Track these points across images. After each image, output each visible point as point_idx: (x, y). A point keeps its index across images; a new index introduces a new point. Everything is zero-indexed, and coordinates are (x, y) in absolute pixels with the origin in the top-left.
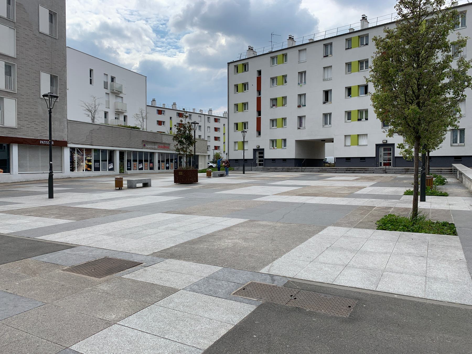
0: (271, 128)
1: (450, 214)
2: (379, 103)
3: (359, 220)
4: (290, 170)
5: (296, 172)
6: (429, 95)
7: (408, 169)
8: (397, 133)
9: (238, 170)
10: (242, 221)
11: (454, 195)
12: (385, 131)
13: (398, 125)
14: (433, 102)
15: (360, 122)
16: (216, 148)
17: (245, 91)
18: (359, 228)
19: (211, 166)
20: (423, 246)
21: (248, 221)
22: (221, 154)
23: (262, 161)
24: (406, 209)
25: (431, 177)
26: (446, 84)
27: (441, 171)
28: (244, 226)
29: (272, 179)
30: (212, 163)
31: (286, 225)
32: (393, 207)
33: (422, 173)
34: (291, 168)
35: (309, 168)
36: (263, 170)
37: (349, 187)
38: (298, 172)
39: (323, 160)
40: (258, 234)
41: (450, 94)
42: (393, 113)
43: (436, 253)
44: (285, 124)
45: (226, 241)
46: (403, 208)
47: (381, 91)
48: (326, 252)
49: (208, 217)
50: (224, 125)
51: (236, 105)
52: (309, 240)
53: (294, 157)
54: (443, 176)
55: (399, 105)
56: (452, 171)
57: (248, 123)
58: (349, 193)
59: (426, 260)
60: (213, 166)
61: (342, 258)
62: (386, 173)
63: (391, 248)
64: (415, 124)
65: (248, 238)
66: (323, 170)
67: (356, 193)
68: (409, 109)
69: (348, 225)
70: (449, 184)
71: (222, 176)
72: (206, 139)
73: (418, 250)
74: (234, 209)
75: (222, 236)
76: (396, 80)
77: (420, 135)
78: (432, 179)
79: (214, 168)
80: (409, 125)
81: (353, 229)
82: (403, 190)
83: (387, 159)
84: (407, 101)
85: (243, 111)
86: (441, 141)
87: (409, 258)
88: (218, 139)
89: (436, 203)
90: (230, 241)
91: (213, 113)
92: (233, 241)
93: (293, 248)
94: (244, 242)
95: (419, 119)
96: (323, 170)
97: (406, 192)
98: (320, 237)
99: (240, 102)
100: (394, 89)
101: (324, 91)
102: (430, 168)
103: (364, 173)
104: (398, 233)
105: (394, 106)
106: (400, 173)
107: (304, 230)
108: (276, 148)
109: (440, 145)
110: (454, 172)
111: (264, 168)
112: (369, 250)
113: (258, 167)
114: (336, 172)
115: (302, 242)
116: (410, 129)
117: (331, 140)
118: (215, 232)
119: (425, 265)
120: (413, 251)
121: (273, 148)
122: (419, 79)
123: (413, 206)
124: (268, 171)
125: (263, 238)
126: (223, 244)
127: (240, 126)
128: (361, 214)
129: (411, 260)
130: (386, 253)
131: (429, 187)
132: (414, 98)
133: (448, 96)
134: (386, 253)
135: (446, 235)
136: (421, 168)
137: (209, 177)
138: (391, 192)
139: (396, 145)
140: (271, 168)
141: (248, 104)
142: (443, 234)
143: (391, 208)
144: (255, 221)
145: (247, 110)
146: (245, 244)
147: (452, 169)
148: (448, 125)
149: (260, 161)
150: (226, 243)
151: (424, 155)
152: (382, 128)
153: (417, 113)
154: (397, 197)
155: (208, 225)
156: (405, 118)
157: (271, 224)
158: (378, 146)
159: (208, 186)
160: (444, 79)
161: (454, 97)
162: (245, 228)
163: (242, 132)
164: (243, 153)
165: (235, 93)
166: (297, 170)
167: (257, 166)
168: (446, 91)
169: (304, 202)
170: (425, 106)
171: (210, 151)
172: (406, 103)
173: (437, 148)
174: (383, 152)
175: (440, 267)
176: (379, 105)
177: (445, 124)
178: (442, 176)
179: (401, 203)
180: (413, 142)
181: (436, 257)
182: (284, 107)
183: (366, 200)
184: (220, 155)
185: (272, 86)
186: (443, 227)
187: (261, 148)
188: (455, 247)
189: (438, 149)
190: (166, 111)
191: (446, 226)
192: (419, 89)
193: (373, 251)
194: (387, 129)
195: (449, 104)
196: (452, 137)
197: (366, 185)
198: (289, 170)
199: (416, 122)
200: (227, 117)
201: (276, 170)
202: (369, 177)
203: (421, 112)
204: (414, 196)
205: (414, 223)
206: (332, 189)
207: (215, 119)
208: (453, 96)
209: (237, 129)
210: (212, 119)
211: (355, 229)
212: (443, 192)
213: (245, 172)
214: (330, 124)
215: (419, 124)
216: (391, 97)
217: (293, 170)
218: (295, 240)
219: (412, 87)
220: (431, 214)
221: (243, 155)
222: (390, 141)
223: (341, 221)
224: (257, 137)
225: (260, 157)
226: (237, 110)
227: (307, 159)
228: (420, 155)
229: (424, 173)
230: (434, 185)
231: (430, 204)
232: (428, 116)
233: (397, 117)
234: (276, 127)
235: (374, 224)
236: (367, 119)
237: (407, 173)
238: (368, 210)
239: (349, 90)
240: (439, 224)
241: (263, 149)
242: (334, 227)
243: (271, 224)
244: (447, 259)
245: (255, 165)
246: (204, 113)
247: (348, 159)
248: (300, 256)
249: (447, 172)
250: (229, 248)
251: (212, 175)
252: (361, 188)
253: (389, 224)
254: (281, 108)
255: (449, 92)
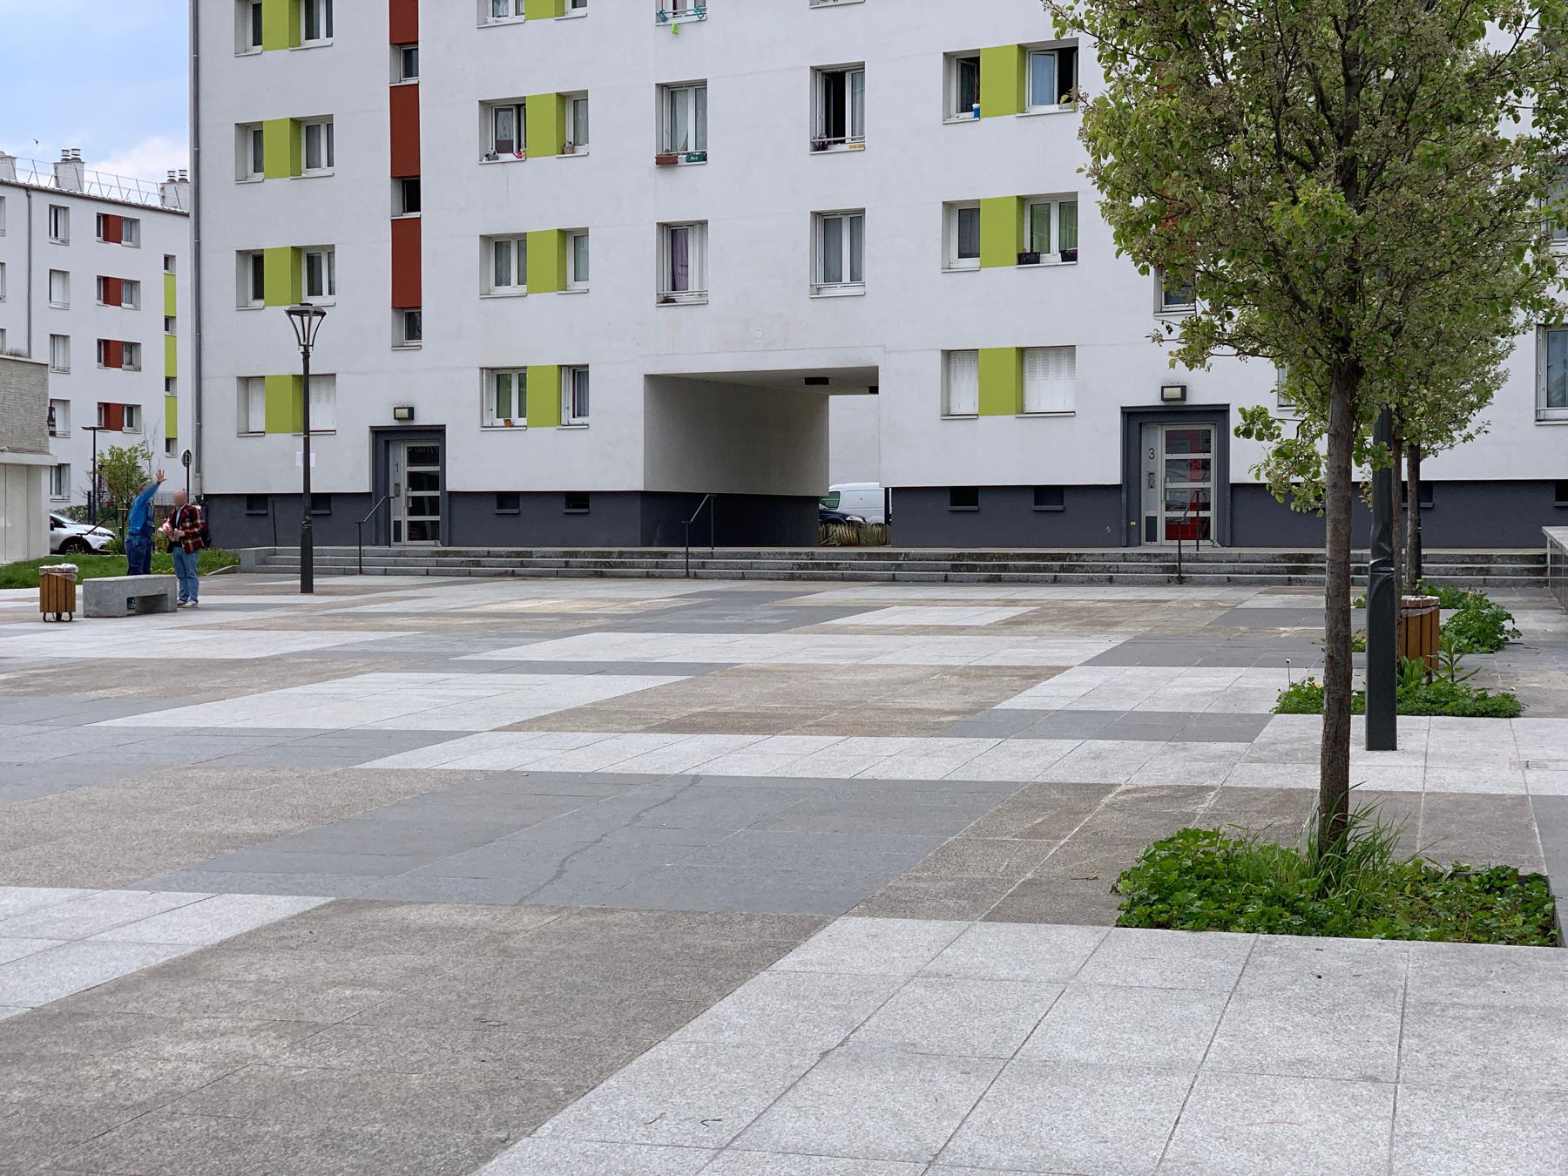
0: (486, 295)
1: (1524, 821)
2: (1124, 161)
3: (1020, 870)
4: (617, 565)
5: (648, 576)
6: (1404, 122)
7: (1306, 558)
8: (1230, 342)
9: (264, 566)
10: (282, 907)
11: (1551, 709)
12: (1166, 335)
13: (1237, 294)
14: (1430, 163)
15: (1029, 271)
16: (113, 416)
17: (311, 43)
18: (1019, 919)
19: (76, 544)
20: (1374, 1012)
21: (322, 907)
22: (148, 457)
23: (433, 506)
24: (1288, 798)
25: (1426, 605)
26: (1500, 60)
27: (1482, 569)
28: (293, 943)
29: (492, 626)
30: (81, 521)
31: (576, 922)
32: (1213, 788)
33: (1373, 579)
34: (621, 554)
35: (734, 556)
36: (440, 570)
37: (965, 673)
38: (661, 577)
39: (816, 500)
40: (389, 993)
41: (1517, 119)
42: (1206, 224)
43: (1448, 1052)
44: (581, 272)
45: (169, 1049)
46: (1268, 793)
47: (1138, 85)
48: (816, 1078)
49: (44, 891)
50: (168, 260)
51: (253, 134)
52: (714, 1009)
53: (633, 480)
54: (1496, 599)
55: (1243, 174)
56: (1542, 571)
57: (331, 255)
58: (968, 707)
59: (1391, 1096)
60: (90, 538)
61: (908, 1114)
62: (1181, 581)
63: (1198, 1036)
64: (1329, 293)
65: (319, 1019)
66: (818, 566)
67: (1005, 705)
68: (1295, 201)
69: (951, 903)
70: (1527, 647)
71: (149, 605)
72: (41, 354)
73: (1346, 1039)
74: (231, 829)
75: (140, 1015)
76: (1220, 22)
77: (1359, 359)
78: (1434, 616)
79: (95, 552)
80: (1297, 299)
81: (980, 927)
82: (1274, 681)
83: (1187, 499)
84: (1286, 154)
85: (296, 173)
86: (1485, 396)
87: (1299, 1091)
88: (126, 357)
89: (1451, 758)
90: (190, 1048)
91: (88, 176)
92: (215, 1044)
93: (612, 1070)
94: (292, 1048)
95: (1351, 261)
96: (818, 566)
97: (1288, 695)
98: (783, 986)
99: (275, 111)
100: (1213, 79)
101: (816, 70)
102: (1424, 552)
103: (1055, 581)
104: (1237, 941)
105: (1213, 182)
106: (1262, 578)
107: (687, 946)
108: (523, 421)
109: (1478, 418)
110: (1555, 572)
111: (446, 554)
112: (1069, 1052)
113: (407, 545)
114: (893, 580)
115: (671, 1028)
116: (1302, 321)
117: (865, 381)
118: (89, 994)
119: (1382, 1127)
120: (1318, 1047)
121: (501, 422)
122: (1351, 21)
123: (1323, 779)
124: (472, 570)
125: (420, 1018)
126: (143, 1073)
127: (277, 274)
128: (1034, 833)
129: (1306, 1106)
130: (1169, 1068)
131: (1413, 666)
132: (1328, 136)
133: (1507, 130)
134: (1169, 1068)
135: (1501, 947)
136: (1369, 551)
137: (59, 619)
138: (1206, 694)
139: (1236, 420)
140: (489, 554)
141: (330, 127)
142: (1488, 941)
143: (1202, 790)
144: (371, 904)
145: (329, 171)
146: (293, 1062)
147: (1545, 556)
148: (1509, 304)
149: (417, 506)
150: (168, 1060)
151: (1385, 476)
152: (1159, 311)
153: (1336, 229)
154: (1242, 727)
155: (39, 945)
156: (1275, 255)
157: (482, 917)
158: (1135, 419)
159: (47, 680)
160: (1484, 32)
161: (1538, 142)
162: (302, 959)
163: (290, 313)
164: (300, 454)
165: (240, 52)
166: (657, 566)
167: (398, 538)
168: (1499, 100)
169: (693, 772)
170: (1383, 186)
171: (66, 435)
172: (1281, 167)
173: (1464, 432)
174: (1162, 456)
175: (1463, 1133)
176: (1128, 170)
177: (1494, 297)
178: (1491, 599)
179: (1259, 760)
180: (1322, 400)
181: (1445, 1075)
182: (568, 163)
183: (1066, 745)
184: (140, 462)
185: (491, 20)
186: (1490, 898)
187: (422, 419)
188: (1545, 1013)
189: (1470, 437)
190: (142, 224)
191: (1501, 889)
192: (1353, 84)
193: (1093, 1059)
194: (1176, 321)
195: (1517, 179)
196: (1543, 373)
197: (1065, 658)
198: (609, 565)
199: (1334, 277)
200: (187, 207)
201: (522, 565)
202: (1083, 609)
203: (1360, 220)
204: (1326, 719)
205: (1327, 879)
206: (866, 683)
207: (106, 217)
208: (1537, 133)
209: (259, 294)
210: (83, 220)
211: (994, 927)
212: (1490, 694)
213: (316, 581)
214: (856, 276)
215: (1353, 292)
216: (1195, 128)
217: (632, 566)
218: (631, 1013)
219: (1312, 69)
220: (1426, 823)
221: (300, 464)
222: (1204, 388)
223: (912, 884)
224: (397, 347)
225: (416, 481)
226: (258, 167)
227: (720, 498)
228: (1361, 473)
229: (1389, 581)
230: (1442, 654)
231: (1422, 762)
232: (1401, 244)
233: (1227, 250)
234: (523, 289)
235: (1103, 891)
236: (1069, 256)
237: (1301, 582)
238: (1070, 811)
239: (967, 68)
240: (1467, 879)
241: (439, 431)
242: (868, 920)
243: (482, 917)
244: (1506, 1084)
245: (386, 533)
246: (22, 179)
247: (964, 496)
248: (657, 1114)
249: (1516, 572)
250: (181, 1096)
251: (79, 603)
252: (1033, 675)
253: (1191, 888)
254: (553, 162)
255: (1511, 110)
